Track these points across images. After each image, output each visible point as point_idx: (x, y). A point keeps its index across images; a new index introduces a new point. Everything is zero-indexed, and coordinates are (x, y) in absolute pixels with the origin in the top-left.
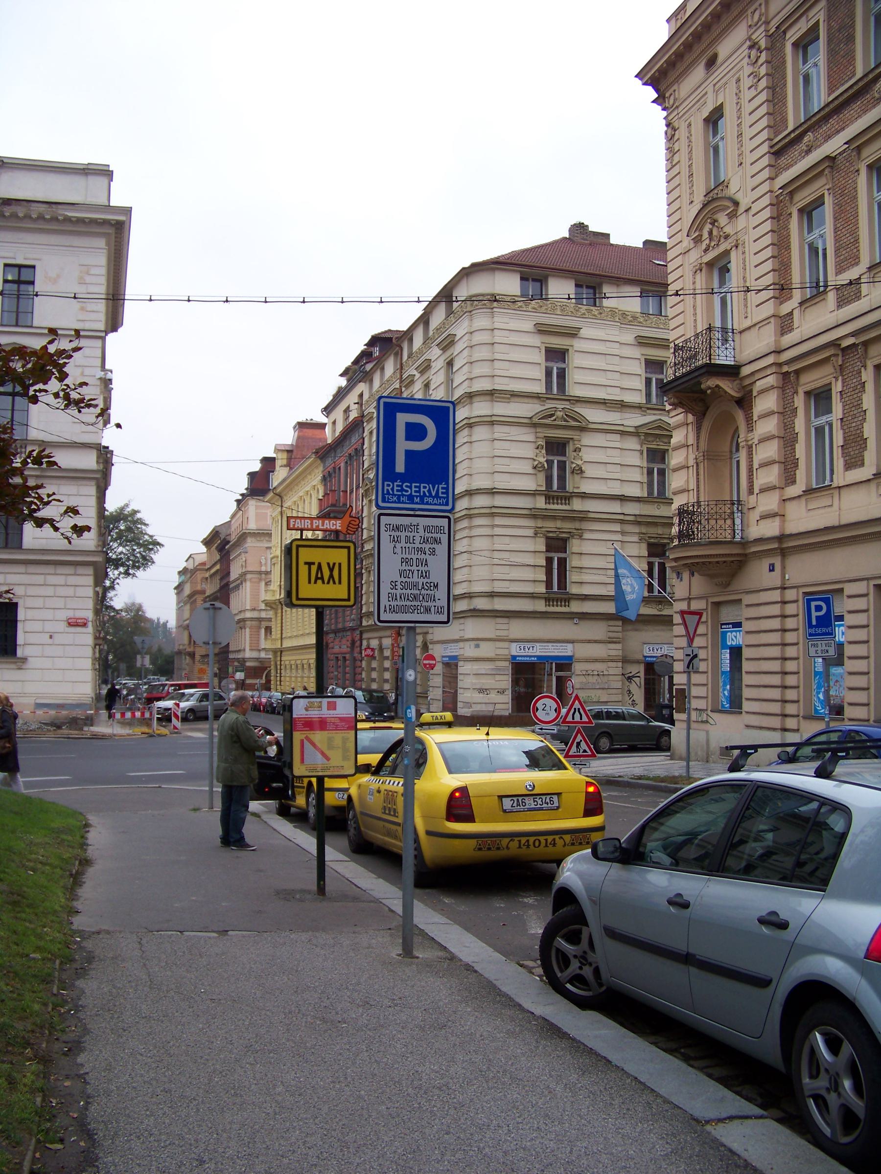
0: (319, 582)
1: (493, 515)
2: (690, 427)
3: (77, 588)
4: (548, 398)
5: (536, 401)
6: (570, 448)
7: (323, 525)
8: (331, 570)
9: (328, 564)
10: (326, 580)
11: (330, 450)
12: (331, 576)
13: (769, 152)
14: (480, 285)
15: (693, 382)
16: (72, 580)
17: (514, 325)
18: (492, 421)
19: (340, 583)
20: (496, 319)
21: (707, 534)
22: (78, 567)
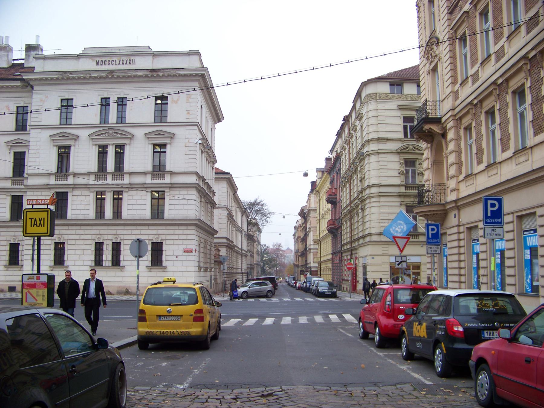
0: (35, 226)
1: (379, 196)
2: (429, 149)
3: (179, 235)
4: (405, 140)
5: (399, 142)
6: (417, 163)
7: (42, 202)
8: (40, 221)
9: (39, 218)
10: (38, 226)
11: (331, 170)
12: (40, 223)
13: (447, 13)
14: (370, 90)
15: (420, 127)
16: (177, 232)
17: (388, 106)
18: (378, 153)
19: (44, 226)
20: (378, 105)
21: (436, 200)
22: (137, 226)
